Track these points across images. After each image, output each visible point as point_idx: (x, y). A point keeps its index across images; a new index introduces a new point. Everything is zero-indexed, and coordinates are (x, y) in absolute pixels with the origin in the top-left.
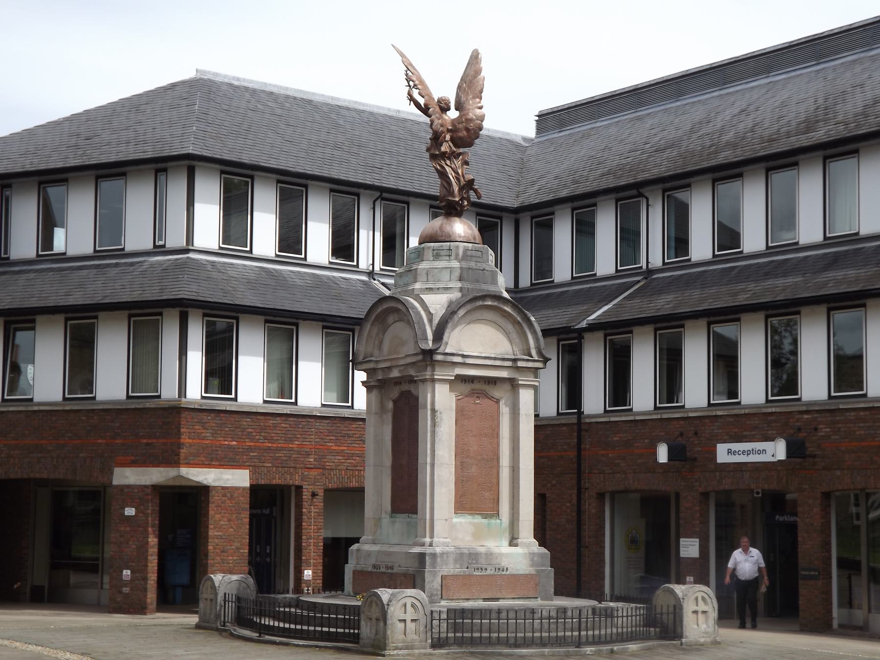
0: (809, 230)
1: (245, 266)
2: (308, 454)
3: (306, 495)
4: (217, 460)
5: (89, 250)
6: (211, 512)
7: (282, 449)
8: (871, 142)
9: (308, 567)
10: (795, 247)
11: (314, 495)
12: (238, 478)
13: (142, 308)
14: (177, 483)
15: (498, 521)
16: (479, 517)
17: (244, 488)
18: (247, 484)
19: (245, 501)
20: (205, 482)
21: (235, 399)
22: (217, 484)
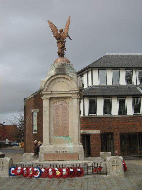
0: (96, 83)
1: (125, 88)
2: (115, 125)
3: (115, 134)
4: (92, 128)
5: (125, 84)
6: (91, 139)
7: (108, 125)
8: (122, 69)
9: (116, 150)
10: (120, 85)
11: (117, 134)
12: (98, 132)
13: (122, 96)
14: (84, 133)
15: (69, 138)
16: (63, 137)
17: (99, 134)
18: (100, 133)
19: (99, 137)
20: (89, 133)
21: (97, 115)
22: (92, 133)
